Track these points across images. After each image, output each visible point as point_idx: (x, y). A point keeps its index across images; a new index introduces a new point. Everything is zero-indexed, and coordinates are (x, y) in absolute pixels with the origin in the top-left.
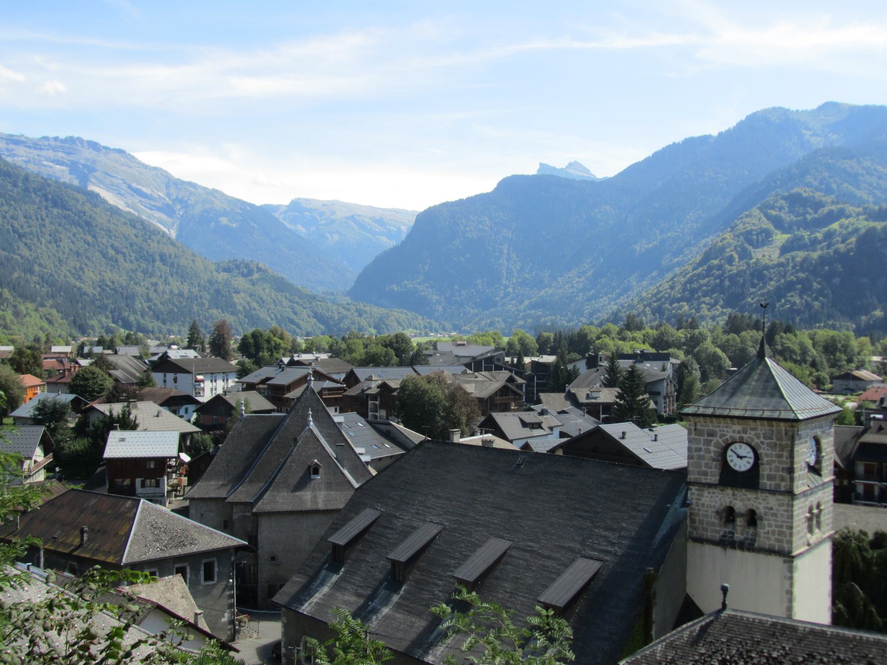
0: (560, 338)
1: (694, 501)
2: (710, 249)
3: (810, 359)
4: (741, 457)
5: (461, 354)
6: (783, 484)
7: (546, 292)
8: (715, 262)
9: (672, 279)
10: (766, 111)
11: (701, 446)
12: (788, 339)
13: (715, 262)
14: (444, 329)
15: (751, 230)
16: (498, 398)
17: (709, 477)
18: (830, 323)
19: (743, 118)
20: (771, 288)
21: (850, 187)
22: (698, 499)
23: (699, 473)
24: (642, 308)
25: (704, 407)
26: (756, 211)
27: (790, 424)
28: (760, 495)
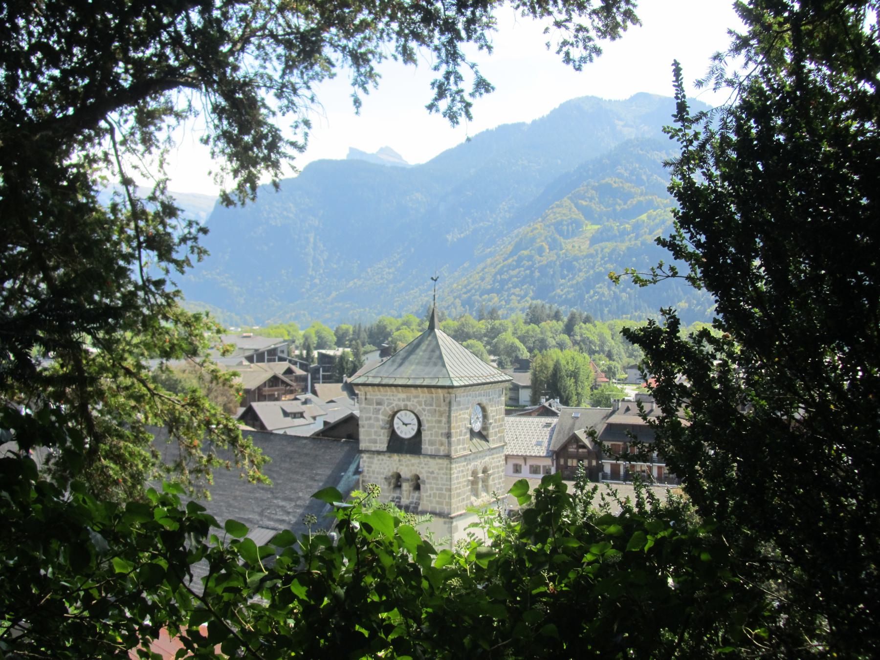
0: (359, 331)
1: (366, 469)
2: (521, 240)
3: (606, 349)
4: (406, 425)
5: (247, 347)
6: (442, 448)
7: (355, 283)
8: (525, 253)
9: (483, 269)
10: (579, 99)
11: (371, 415)
12: (587, 329)
13: (525, 253)
14: (246, 323)
15: (562, 220)
16: (267, 388)
17: (378, 445)
18: (637, 314)
19: (557, 106)
20: (580, 280)
21: (659, 178)
22: (369, 467)
23: (371, 441)
24: (452, 300)
25: (374, 377)
26: (566, 201)
27: (446, 390)
28: (422, 459)
